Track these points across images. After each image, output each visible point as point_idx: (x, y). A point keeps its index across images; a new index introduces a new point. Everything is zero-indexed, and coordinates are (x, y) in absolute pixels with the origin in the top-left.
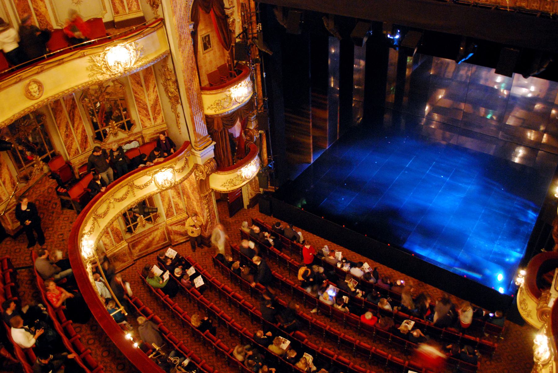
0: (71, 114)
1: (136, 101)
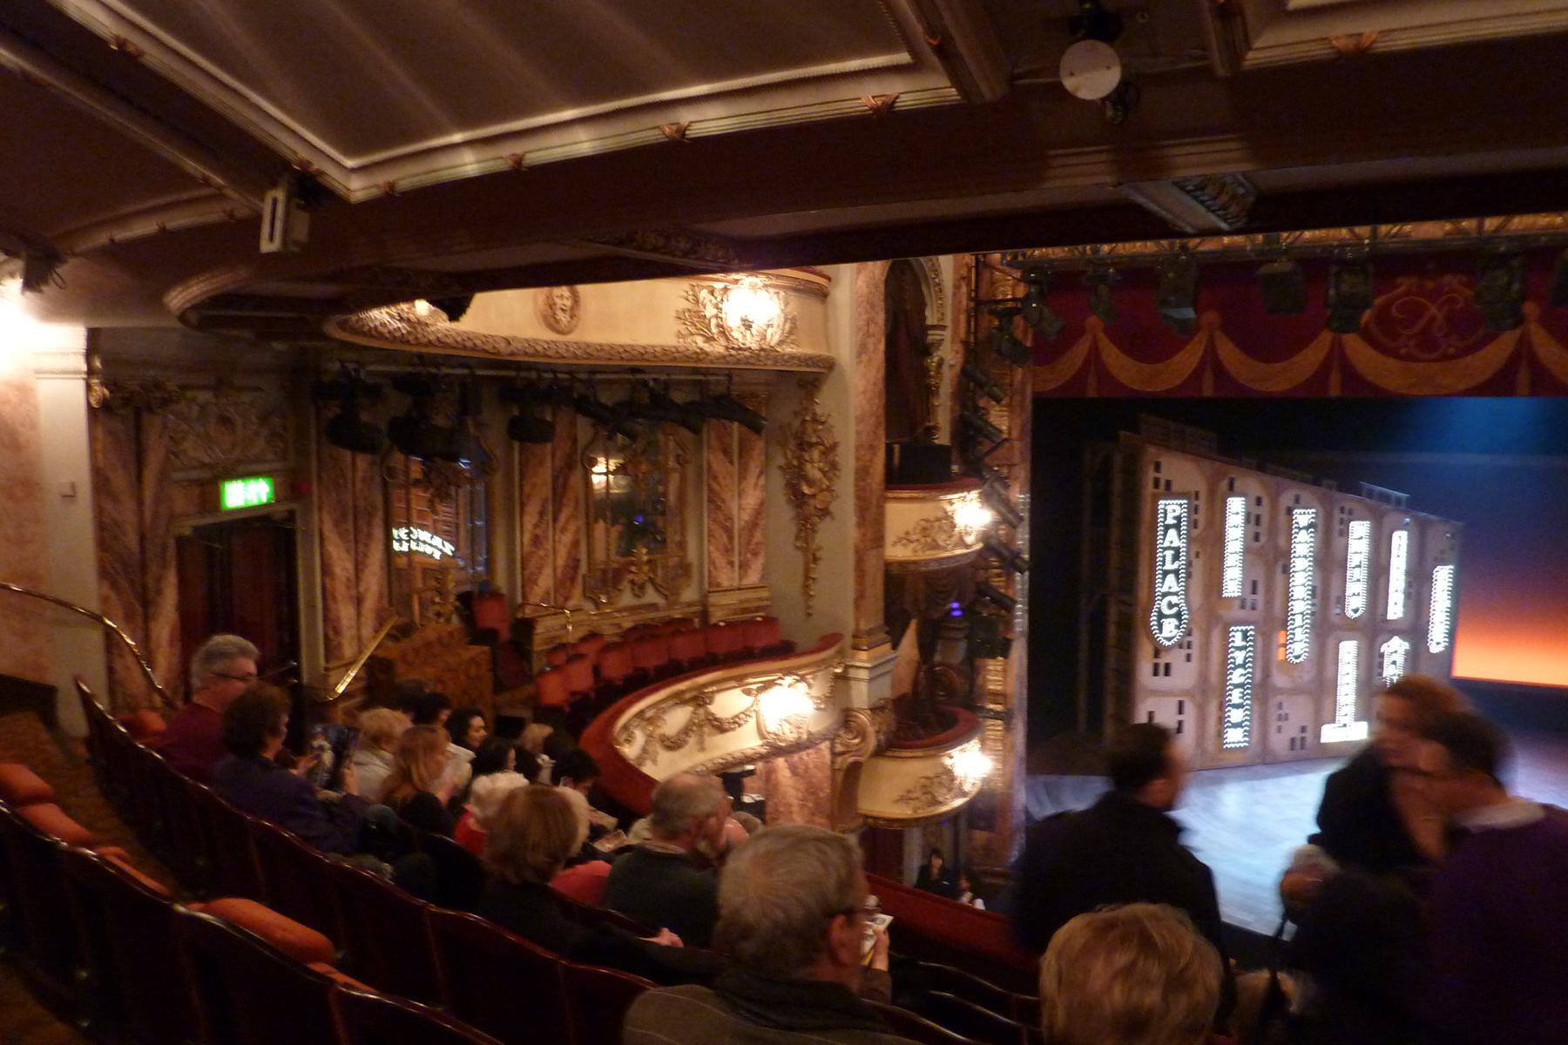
0: (561, 480)
1: (710, 501)
